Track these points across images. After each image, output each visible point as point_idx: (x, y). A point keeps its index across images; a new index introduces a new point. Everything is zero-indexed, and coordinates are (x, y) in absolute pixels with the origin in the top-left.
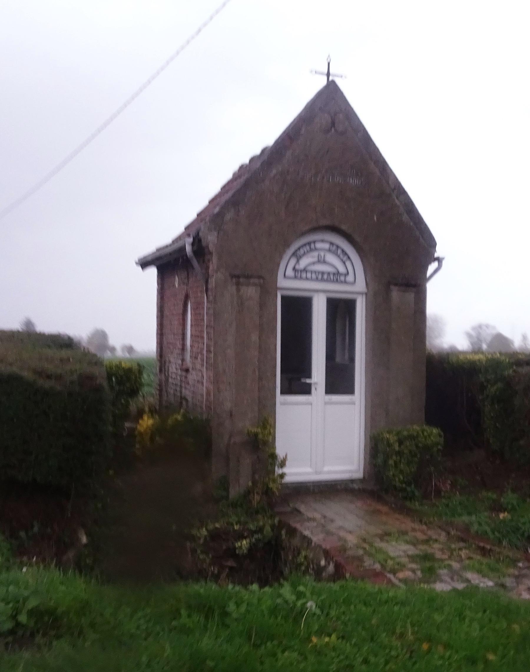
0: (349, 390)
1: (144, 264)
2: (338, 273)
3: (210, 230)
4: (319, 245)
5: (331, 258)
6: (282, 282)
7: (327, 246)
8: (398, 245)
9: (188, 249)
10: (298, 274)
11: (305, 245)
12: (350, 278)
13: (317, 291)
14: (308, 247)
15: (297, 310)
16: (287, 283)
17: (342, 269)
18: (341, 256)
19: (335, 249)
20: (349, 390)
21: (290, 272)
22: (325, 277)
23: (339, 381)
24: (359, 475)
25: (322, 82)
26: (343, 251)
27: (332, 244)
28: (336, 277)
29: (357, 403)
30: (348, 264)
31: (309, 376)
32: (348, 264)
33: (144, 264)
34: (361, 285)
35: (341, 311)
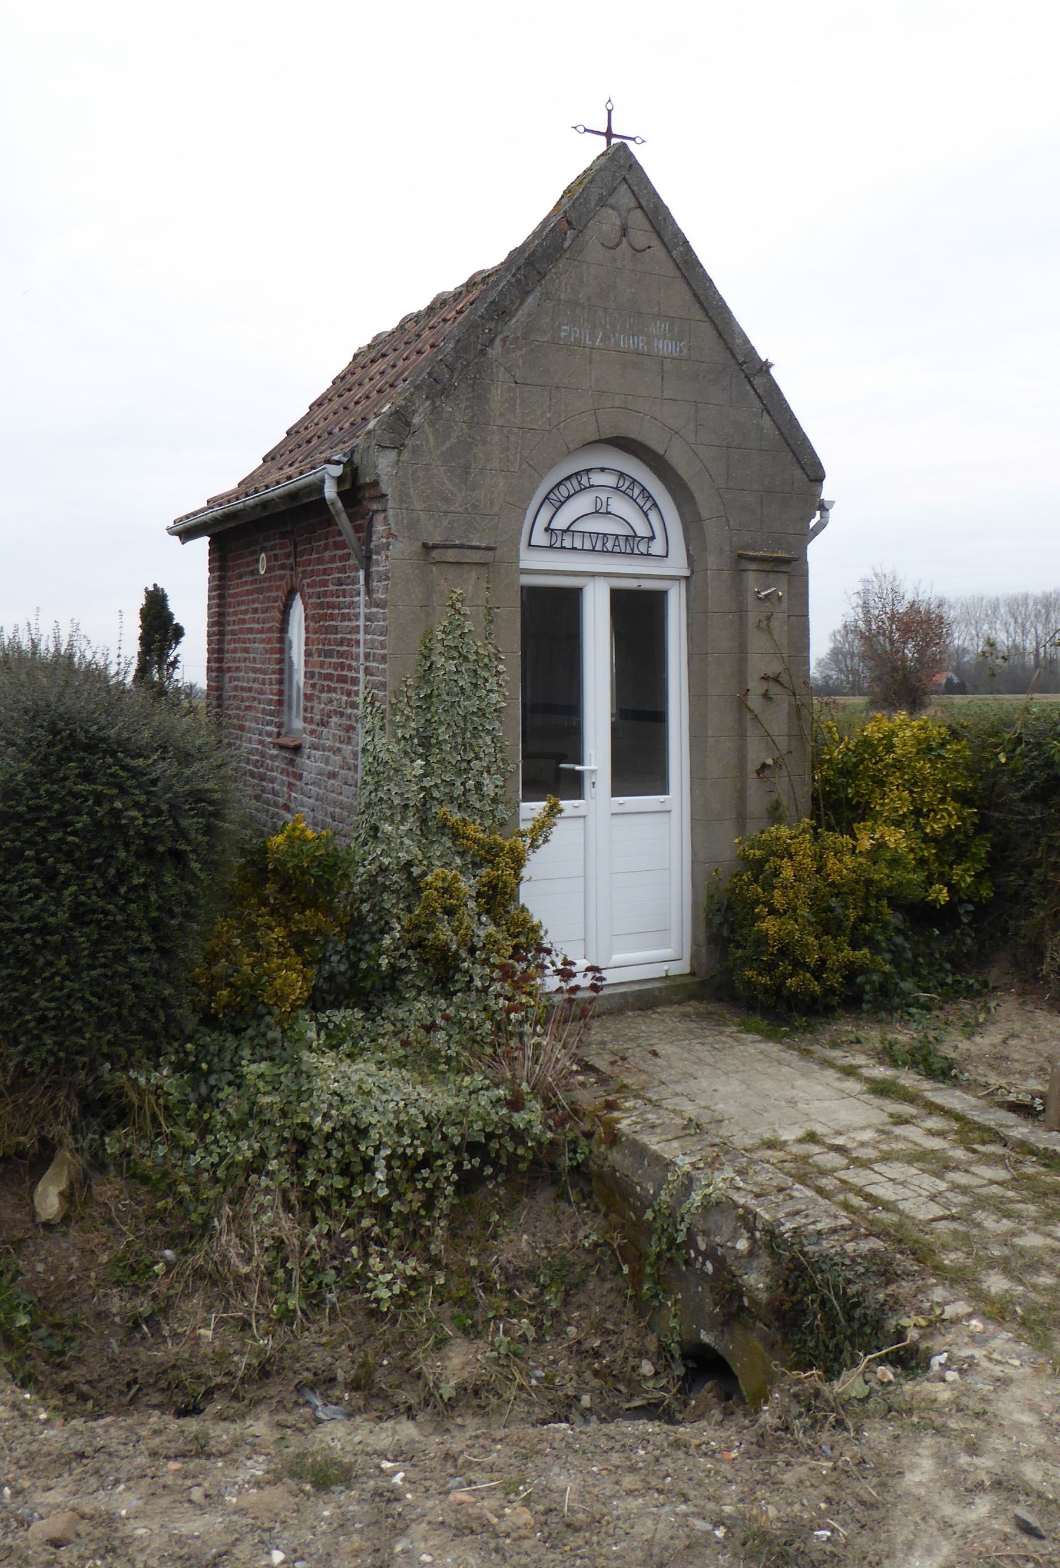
0: (658, 783)
1: (186, 532)
2: (632, 538)
3: (338, 514)
4: (597, 479)
5: (620, 506)
6: (529, 560)
7: (610, 480)
8: (759, 477)
9: (330, 491)
10: (558, 540)
11: (568, 478)
12: (657, 547)
13: (593, 575)
14: (575, 482)
15: (552, 616)
16: (541, 564)
17: (642, 530)
18: (641, 502)
19: (626, 487)
20: (658, 783)
21: (540, 538)
22: (609, 546)
23: (639, 764)
24: (682, 967)
25: (600, 145)
26: (644, 489)
27: (622, 475)
28: (630, 544)
29: (675, 815)
30: (653, 516)
31: (580, 761)
32: (653, 516)
33: (186, 532)
34: (677, 564)
35: (638, 616)
